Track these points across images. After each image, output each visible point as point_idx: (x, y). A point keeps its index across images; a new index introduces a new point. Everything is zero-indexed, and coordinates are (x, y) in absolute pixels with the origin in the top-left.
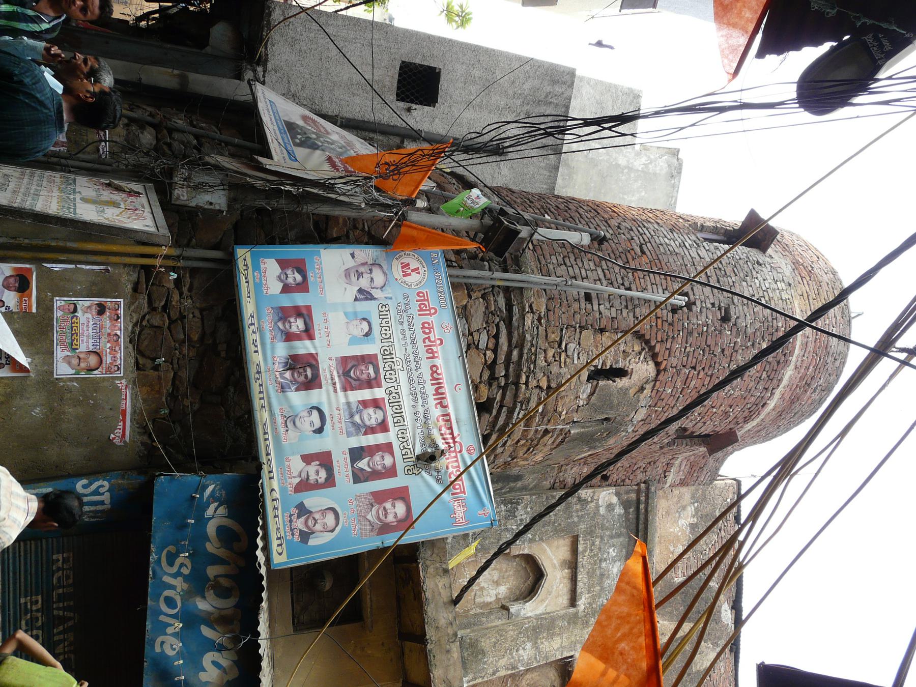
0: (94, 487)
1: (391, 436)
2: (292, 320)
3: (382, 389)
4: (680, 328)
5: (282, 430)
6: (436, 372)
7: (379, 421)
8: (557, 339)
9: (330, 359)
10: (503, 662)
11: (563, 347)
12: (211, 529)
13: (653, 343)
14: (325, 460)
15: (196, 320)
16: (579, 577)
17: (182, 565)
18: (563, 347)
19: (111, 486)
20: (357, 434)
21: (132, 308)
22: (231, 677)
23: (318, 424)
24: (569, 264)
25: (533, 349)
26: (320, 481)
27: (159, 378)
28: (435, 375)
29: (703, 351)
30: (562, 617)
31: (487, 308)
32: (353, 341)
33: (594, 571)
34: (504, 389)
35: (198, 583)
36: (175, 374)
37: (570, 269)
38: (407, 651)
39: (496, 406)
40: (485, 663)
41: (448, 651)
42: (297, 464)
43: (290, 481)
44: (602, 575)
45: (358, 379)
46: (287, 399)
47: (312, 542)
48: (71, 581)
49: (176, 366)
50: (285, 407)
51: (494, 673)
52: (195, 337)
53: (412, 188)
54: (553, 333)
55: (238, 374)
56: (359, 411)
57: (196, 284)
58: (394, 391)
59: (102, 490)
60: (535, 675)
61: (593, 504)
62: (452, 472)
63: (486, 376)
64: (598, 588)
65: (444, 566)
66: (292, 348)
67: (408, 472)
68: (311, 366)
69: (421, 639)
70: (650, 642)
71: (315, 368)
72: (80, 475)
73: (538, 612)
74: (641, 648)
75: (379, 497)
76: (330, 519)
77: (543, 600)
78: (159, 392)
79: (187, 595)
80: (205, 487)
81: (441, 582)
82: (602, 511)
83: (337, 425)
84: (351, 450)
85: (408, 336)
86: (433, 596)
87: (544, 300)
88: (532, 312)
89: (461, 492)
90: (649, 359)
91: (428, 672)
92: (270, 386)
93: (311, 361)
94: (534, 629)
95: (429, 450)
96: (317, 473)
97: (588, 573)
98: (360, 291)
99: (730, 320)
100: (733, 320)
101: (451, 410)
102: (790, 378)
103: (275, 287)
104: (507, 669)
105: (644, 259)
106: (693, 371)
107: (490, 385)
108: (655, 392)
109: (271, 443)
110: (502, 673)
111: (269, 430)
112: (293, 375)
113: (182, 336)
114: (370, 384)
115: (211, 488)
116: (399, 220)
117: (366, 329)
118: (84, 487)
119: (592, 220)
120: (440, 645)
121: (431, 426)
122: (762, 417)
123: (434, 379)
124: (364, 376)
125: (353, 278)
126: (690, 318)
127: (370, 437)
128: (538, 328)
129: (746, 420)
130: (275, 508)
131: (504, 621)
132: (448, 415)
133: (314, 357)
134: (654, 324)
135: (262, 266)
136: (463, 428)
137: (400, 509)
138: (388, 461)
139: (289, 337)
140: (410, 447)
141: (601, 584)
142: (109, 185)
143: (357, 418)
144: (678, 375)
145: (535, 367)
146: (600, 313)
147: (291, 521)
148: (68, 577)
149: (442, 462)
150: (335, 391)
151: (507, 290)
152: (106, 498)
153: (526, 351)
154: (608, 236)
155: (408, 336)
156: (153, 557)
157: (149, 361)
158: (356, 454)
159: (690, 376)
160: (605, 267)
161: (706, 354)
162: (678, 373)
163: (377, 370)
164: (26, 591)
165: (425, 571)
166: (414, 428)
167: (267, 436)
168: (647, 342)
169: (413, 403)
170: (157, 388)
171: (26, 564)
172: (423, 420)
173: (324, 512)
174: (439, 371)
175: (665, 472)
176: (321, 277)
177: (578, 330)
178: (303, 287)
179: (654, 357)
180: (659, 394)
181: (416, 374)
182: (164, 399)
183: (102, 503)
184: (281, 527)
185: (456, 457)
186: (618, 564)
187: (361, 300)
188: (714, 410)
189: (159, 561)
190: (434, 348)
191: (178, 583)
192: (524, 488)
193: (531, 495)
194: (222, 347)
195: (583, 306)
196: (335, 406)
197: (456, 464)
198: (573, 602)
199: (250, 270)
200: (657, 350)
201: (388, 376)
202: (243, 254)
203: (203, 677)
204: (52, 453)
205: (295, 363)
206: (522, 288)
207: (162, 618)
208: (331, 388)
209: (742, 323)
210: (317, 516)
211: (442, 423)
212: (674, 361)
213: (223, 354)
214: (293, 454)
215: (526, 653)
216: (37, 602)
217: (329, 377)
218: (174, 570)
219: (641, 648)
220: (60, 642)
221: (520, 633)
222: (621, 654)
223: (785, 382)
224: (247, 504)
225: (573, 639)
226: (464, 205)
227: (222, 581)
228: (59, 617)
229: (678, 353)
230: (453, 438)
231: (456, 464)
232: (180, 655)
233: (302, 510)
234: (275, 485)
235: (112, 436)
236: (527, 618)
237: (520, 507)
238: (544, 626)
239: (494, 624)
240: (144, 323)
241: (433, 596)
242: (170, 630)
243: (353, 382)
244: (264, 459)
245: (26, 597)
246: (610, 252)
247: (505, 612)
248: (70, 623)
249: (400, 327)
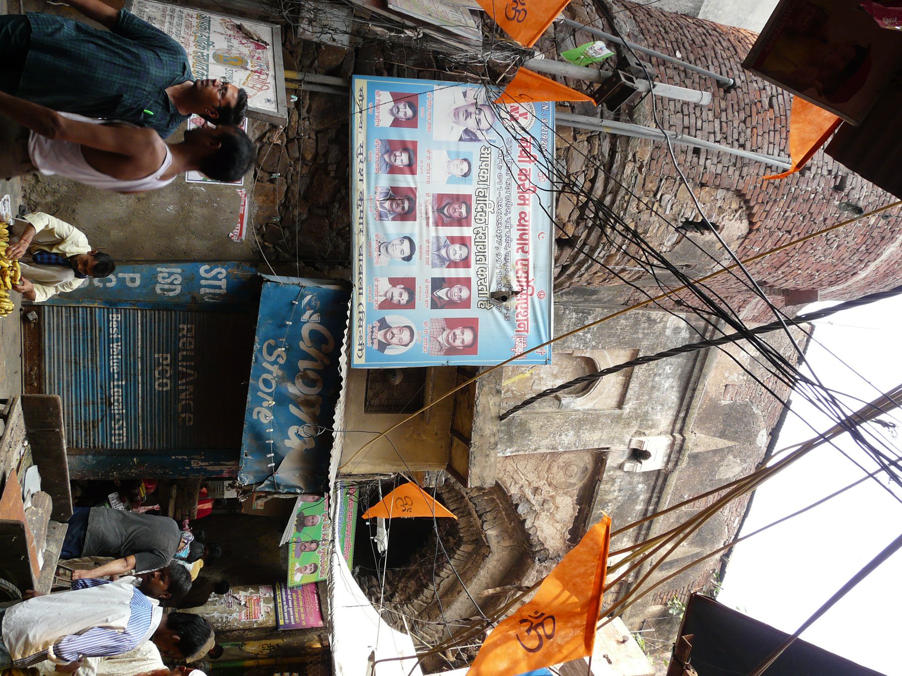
0: (214, 272)
1: (471, 272)
2: (398, 153)
3: (471, 229)
4: (786, 192)
5: (375, 253)
6: (523, 218)
7: (463, 257)
8: (654, 189)
9: (428, 195)
10: (545, 442)
11: (658, 197)
12: (305, 331)
13: (752, 204)
14: (409, 285)
15: (311, 141)
16: (631, 385)
17: (279, 356)
18: (658, 197)
19: (228, 273)
20: (441, 266)
21: (255, 125)
22: (308, 447)
23: (407, 252)
24: (686, 112)
25: (627, 198)
26: (402, 302)
27: (274, 190)
28: (522, 222)
29: (804, 217)
30: (608, 416)
31: (590, 151)
32: (452, 180)
33: (647, 382)
34: (591, 230)
35: (290, 372)
36: (288, 187)
37: (686, 118)
38: (455, 444)
39: (579, 245)
40: (530, 440)
41: (487, 456)
42: (384, 286)
43: (376, 298)
44: (653, 387)
45: (450, 217)
46: (383, 227)
47: (387, 352)
48: (193, 347)
49: (289, 181)
50: (381, 234)
51: (535, 450)
52: (309, 157)
53: (536, 32)
54: (651, 182)
55: (343, 192)
56: (446, 246)
57: (314, 106)
58: (481, 232)
59: (220, 276)
60: (572, 456)
61: (661, 325)
62: (520, 313)
63: (575, 216)
64: (647, 397)
65: (498, 387)
66: (394, 180)
67: (481, 306)
68: (409, 199)
69: (467, 441)
70: (599, 581)
71: (412, 201)
72: (204, 261)
73: (586, 407)
74: (590, 583)
75: (452, 324)
76: (406, 335)
77: (593, 399)
78: (273, 202)
79: (281, 380)
80: (303, 296)
81: (493, 400)
82: (668, 332)
83: (424, 256)
84: (434, 280)
85: (504, 180)
86: (484, 410)
87: (650, 148)
88: (635, 161)
89: (525, 331)
90: (744, 217)
91: (467, 469)
92: (370, 214)
93: (409, 195)
94: (579, 421)
95: (503, 290)
96: (401, 295)
97: (640, 383)
98: (466, 131)
99: (843, 190)
100: (846, 190)
101: (530, 257)
102: (892, 254)
103: (385, 119)
104: (548, 448)
105: (770, 114)
106: (787, 235)
107: (578, 224)
108: (742, 248)
109: (364, 263)
110: (543, 450)
111: (364, 252)
112: (391, 205)
113: (297, 155)
114: (460, 222)
115: (308, 298)
116: (515, 65)
117: (466, 170)
118: (207, 271)
119: (727, 62)
120: (481, 449)
121: (509, 268)
122: (849, 283)
123: (520, 225)
124: (456, 215)
125: (462, 117)
126: (800, 184)
127: (453, 270)
128: (636, 177)
129: (831, 284)
130: (361, 319)
131: (554, 410)
132: (527, 260)
133: (413, 191)
134: (759, 185)
135: (377, 98)
136: (539, 274)
137: (468, 336)
138: (465, 294)
139: (393, 170)
140: (487, 284)
141: (650, 394)
142: (240, 28)
143: (443, 252)
144: (770, 236)
145: (625, 214)
146: (705, 168)
147: (372, 332)
148: (190, 344)
149: (513, 302)
150: (428, 224)
151: (614, 137)
152: (223, 283)
153: (619, 198)
154: (738, 83)
155: (504, 180)
156: (257, 346)
157: (266, 174)
158: (438, 284)
159: (783, 238)
160: (724, 119)
161: (806, 221)
162: (771, 234)
163: (469, 210)
164: (159, 349)
165: (481, 389)
166: (494, 268)
167: (361, 258)
168: (747, 202)
169: (497, 245)
170: (271, 198)
171: (159, 328)
172: (504, 262)
173: (401, 329)
174: (526, 218)
175: (740, 307)
176: (431, 114)
177: (677, 182)
178: (412, 122)
179: (750, 216)
180: (746, 250)
181: (505, 218)
182: (277, 208)
183: (220, 287)
184: (364, 335)
185: (527, 299)
186: (671, 380)
187: (465, 140)
188: (800, 272)
189: (260, 351)
190: (527, 196)
191: (275, 369)
192: (599, 301)
193: (603, 308)
194: (332, 168)
195: (689, 159)
196: (425, 238)
197: (525, 306)
198: (620, 404)
199: (365, 101)
200: (754, 211)
201: (479, 217)
202: (360, 84)
203: (287, 443)
204: (181, 242)
205: (394, 194)
206: (629, 137)
207: (260, 394)
208: (424, 222)
209: (855, 195)
210: (395, 331)
211: (520, 266)
212: (769, 223)
213: (332, 174)
214: (382, 276)
215: (568, 439)
216: (167, 359)
217: (424, 211)
218: (273, 358)
219: (590, 583)
220: (183, 391)
221: (566, 422)
222: (574, 585)
223: (884, 257)
224: (336, 313)
225: (613, 435)
226: (586, 54)
227: (309, 372)
228: (183, 373)
229: (776, 216)
230: (528, 282)
231: (525, 306)
232: (272, 424)
233: (383, 324)
234: (363, 300)
235: (231, 234)
236: (575, 411)
237: (590, 317)
238: (590, 420)
239: (545, 411)
240: (265, 140)
241: (484, 410)
242: (265, 404)
243: (445, 219)
244: (356, 282)
245: (159, 353)
246: (735, 102)
247: (556, 402)
248: (191, 378)
249: (498, 171)
